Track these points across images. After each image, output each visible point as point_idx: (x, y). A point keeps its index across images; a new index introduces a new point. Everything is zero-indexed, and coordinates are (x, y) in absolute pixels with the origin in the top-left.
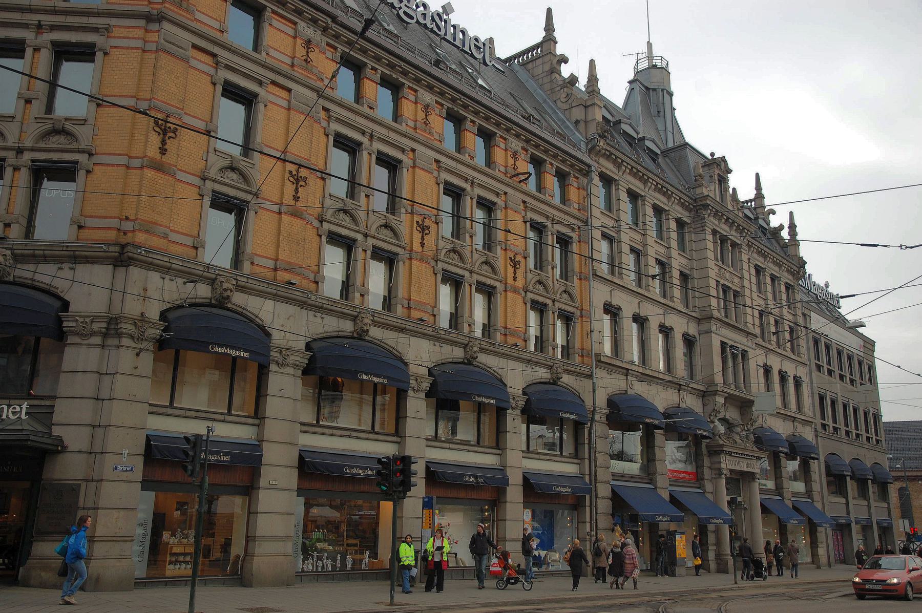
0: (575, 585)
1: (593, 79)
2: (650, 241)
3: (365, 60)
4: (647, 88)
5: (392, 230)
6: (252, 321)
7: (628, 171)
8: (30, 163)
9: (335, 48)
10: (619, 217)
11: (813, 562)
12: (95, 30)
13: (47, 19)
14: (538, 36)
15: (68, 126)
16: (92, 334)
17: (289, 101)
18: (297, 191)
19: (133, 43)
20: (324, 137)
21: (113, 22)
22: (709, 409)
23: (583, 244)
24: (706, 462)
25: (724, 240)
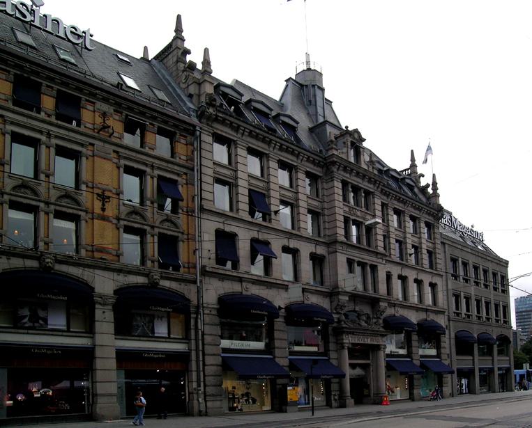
0: (313, 415)
1: (206, 62)
2: (424, 241)
3: (81, 96)
4: (302, 85)
5: (172, 222)
7: (246, 134)
9: (52, 88)
10: (237, 168)
11: (410, 399)
17: (93, 151)
18: (103, 205)
20: (117, 170)
22: (335, 304)
23: (189, 186)
24: (332, 339)
25: (356, 189)
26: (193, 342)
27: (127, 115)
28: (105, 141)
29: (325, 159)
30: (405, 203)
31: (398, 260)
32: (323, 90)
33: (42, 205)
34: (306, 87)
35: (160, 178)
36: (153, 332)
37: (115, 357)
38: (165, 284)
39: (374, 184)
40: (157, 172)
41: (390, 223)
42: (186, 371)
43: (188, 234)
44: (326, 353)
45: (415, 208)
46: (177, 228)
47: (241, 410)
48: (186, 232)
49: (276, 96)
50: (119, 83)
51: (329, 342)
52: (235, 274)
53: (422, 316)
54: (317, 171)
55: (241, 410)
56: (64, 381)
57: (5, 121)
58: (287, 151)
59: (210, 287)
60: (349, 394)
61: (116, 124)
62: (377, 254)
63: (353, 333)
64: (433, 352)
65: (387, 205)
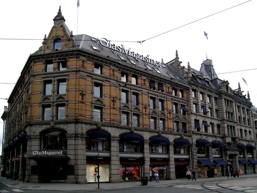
2: (214, 106)
6: (106, 132)
8: (55, 105)
11: (222, 175)
12: (65, 76)
13: (56, 75)
14: (174, 57)
15: (62, 96)
16: (73, 137)
17: (110, 84)
19: (74, 77)
21: (69, 73)
22: (224, 141)
24: (223, 152)
25: (228, 101)
26: (191, 155)
27: (122, 71)
28: (170, 96)
29: (219, 92)
30: (205, 89)
31: (202, 114)
32: (213, 66)
33: (52, 103)
34: (208, 66)
35: (182, 105)
36: (181, 153)
37: (86, 159)
38: (184, 137)
39: (233, 99)
40: (181, 103)
41: (199, 98)
42: (189, 164)
43: (188, 121)
44: (222, 157)
45: (243, 104)
46: (102, 103)
47: (201, 177)
48: (142, 112)
49: (198, 70)
50: (108, 56)
51: (222, 154)
52: (199, 133)
53: (247, 143)
54: (217, 96)
55: (201, 177)
56: (156, 167)
57: (93, 78)
58: (209, 91)
59: (194, 137)
60: (229, 172)
61: (117, 74)
62: (235, 122)
63: (230, 150)
64: (251, 156)
65: (240, 106)
